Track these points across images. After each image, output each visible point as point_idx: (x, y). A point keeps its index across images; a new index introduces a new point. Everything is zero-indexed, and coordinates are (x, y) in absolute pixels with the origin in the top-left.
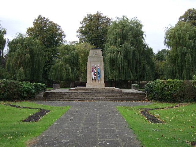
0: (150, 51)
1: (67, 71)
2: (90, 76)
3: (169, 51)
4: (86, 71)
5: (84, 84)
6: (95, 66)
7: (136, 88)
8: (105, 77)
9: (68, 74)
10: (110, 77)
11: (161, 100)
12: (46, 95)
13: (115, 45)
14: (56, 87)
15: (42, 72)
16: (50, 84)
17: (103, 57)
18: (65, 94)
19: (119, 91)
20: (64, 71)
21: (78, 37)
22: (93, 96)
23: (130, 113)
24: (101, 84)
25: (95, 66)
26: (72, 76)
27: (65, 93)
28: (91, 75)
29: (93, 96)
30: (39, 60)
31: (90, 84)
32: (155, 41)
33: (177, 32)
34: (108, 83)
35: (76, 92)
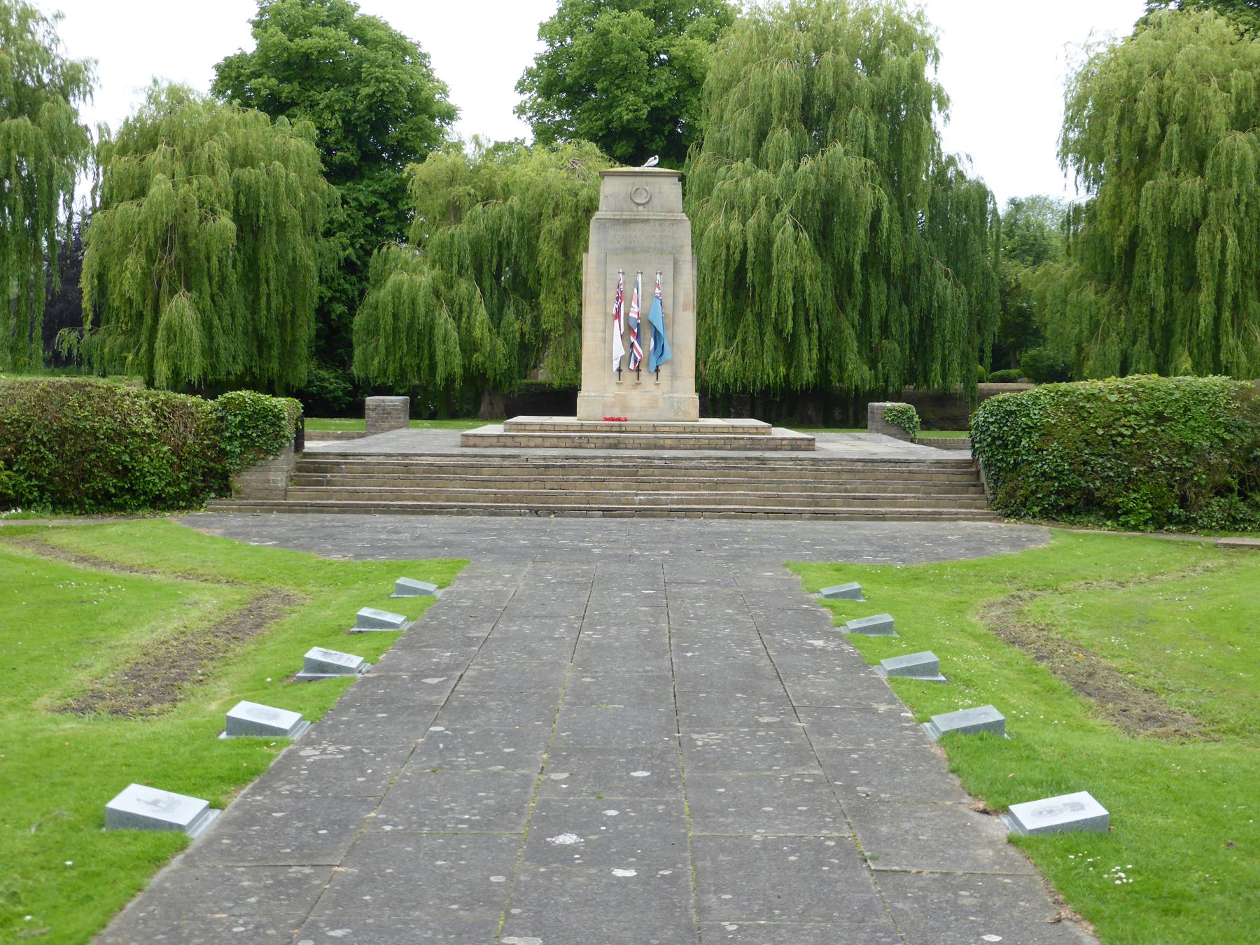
0: (982, 194)
1: (471, 328)
2: (602, 344)
3: (1095, 202)
4: (575, 324)
5: (562, 399)
6: (640, 281)
7: (899, 427)
8: (701, 360)
9: (469, 346)
10: (728, 363)
11: (1089, 512)
12: (313, 471)
13: (758, 162)
14: (385, 421)
15: (307, 329)
16: (347, 406)
17: (689, 223)
18: (438, 471)
19: (794, 445)
20: (443, 318)
21: (524, 117)
22: (633, 479)
23: (912, 602)
24: (671, 397)
25: (640, 281)
26: (496, 351)
27: (431, 460)
28: (607, 341)
29: (633, 479)
30: (294, 269)
31: (599, 393)
32: (1010, 142)
33: (1148, 89)
34: (716, 399)
35: (507, 452)
